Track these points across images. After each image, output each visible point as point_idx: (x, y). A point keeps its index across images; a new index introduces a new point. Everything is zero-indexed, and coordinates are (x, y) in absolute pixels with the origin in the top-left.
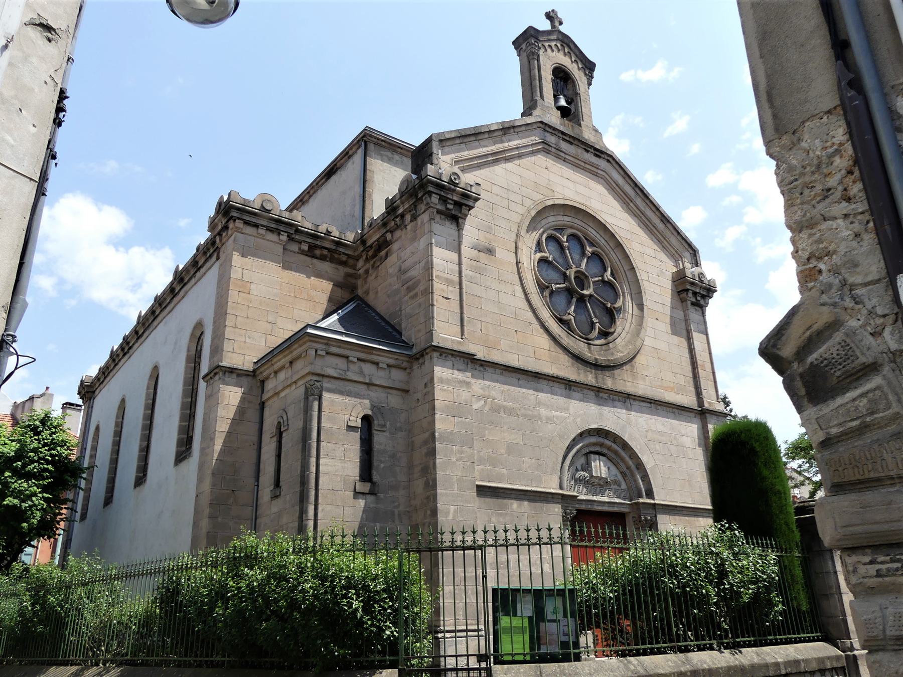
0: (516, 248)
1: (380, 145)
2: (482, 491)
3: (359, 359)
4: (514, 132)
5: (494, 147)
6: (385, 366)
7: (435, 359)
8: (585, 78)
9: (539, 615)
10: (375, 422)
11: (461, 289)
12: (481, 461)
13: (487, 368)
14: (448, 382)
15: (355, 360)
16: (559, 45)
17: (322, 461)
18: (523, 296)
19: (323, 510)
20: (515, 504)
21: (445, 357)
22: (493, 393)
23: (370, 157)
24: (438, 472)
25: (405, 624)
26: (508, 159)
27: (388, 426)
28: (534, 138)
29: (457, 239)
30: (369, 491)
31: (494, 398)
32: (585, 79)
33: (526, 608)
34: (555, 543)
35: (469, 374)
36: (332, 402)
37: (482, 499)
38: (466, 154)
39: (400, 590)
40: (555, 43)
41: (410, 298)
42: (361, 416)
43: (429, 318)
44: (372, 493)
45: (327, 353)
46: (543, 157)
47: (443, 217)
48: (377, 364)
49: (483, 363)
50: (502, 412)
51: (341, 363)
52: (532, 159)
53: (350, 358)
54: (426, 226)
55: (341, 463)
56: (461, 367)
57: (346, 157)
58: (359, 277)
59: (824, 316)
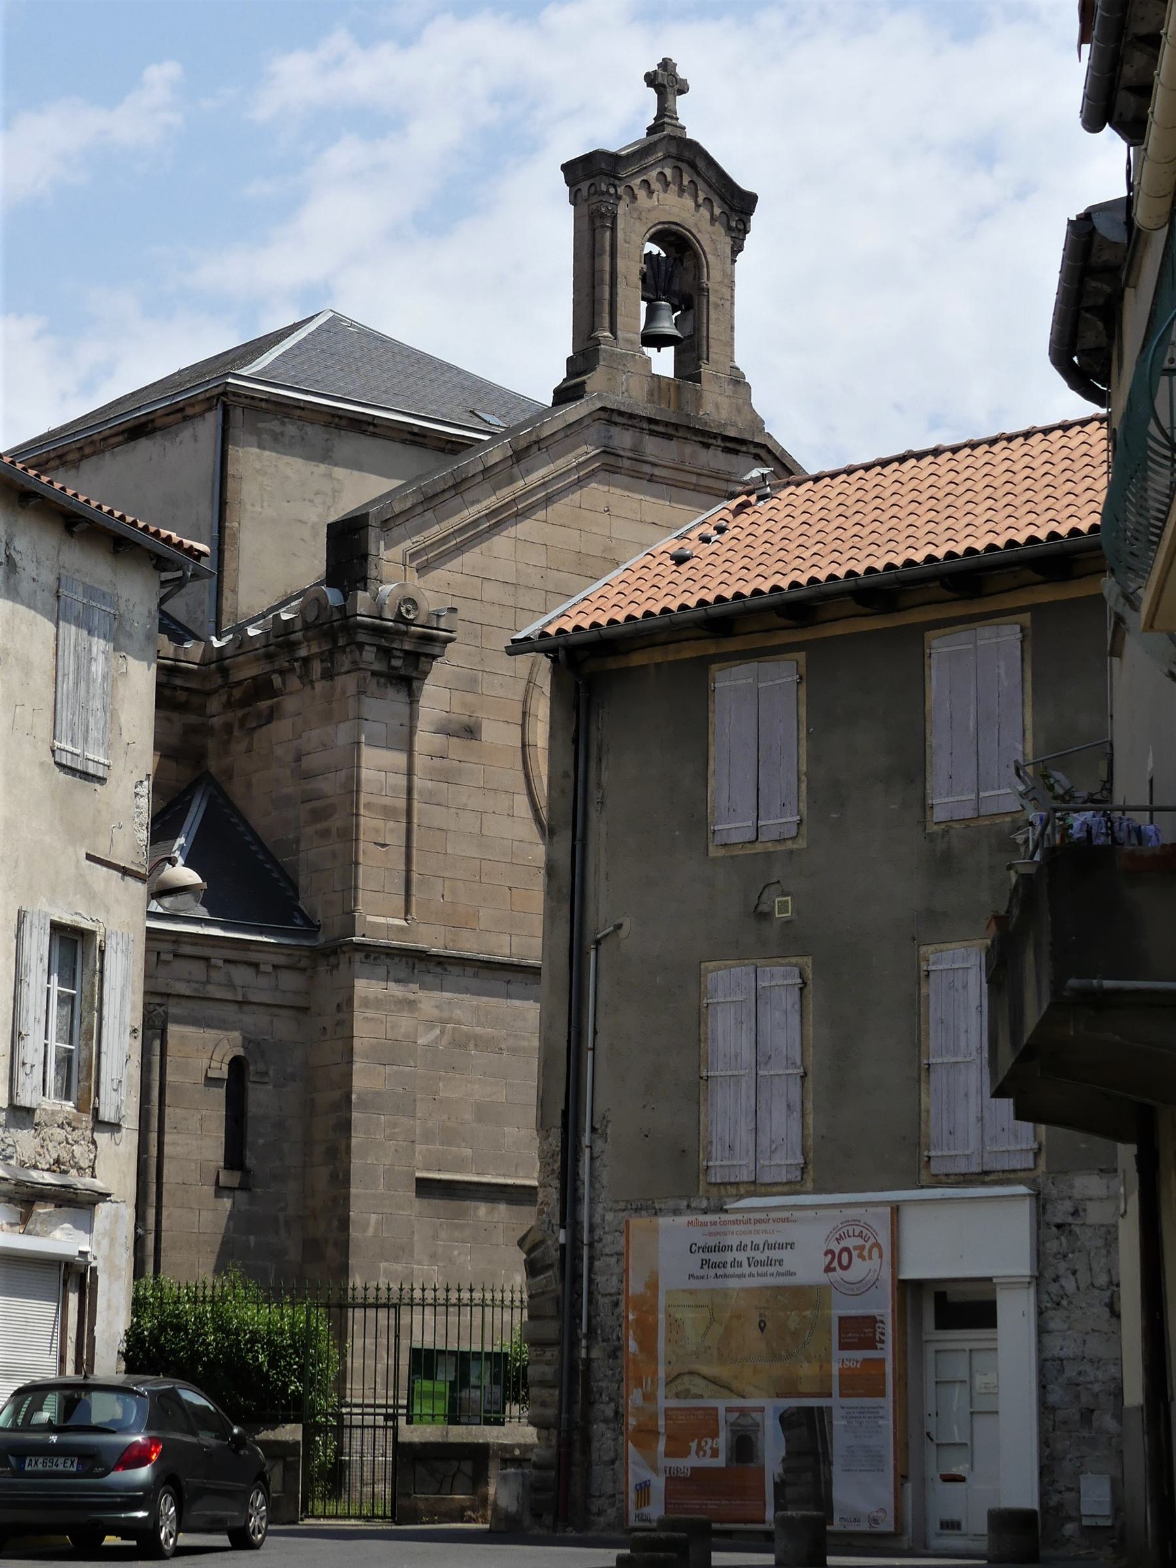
0: (524, 713)
1: (257, 409)
2: (425, 1188)
3: (226, 961)
4: (539, 449)
5: (493, 498)
6: (270, 969)
7: (357, 966)
8: (728, 239)
9: (461, 1381)
10: (252, 1068)
11: (409, 822)
12: (428, 1137)
13: (449, 968)
14: (378, 1003)
15: (220, 963)
16: (668, 172)
17: (167, 1138)
18: (530, 815)
19: (168, 1216)
20: (482, 1210)
21: (375, 959)
22: (458, 1013)
23: (233, 445)
24: (353, 1160)
25: (310, 1382)
26: (520, 516)
27: (271, 1073)
28: (584, 448)
29: (406, 721)
30: (240, 1184)
31: (459, 1023)
32: (725, 243)
33: (446, 1373)
34: (476, 1305)
35: (414, 987)
36: (183, 1038)
37: (426, 1201)
38: (436, 531)
39: (306, 1347)
40: (659, 170)
41: (316, 832)
42: (228, 1059)
43: (350, 889)
44: (244, 1187)
45: (176, 955)
46: (601, 487)
47: (382, 680)
48: (255, 965)
49: (441, 959)
50: (472, 1046)
51: (197, 970)
52: (576, 497)
53: (213, 961)
54: (351, 702)
55: (197, 1139)
56: (402, 975)
57: (179, 415)
58: (210, 731)
59: (538, 1236)
